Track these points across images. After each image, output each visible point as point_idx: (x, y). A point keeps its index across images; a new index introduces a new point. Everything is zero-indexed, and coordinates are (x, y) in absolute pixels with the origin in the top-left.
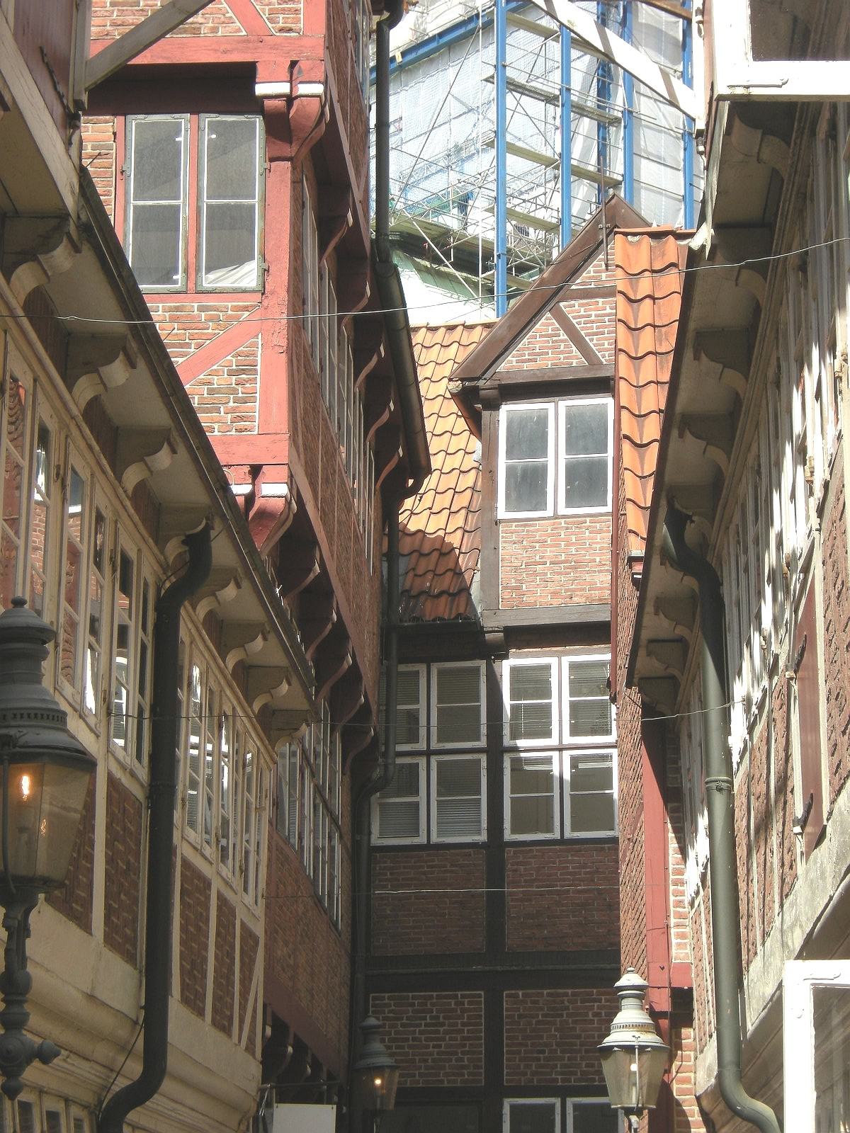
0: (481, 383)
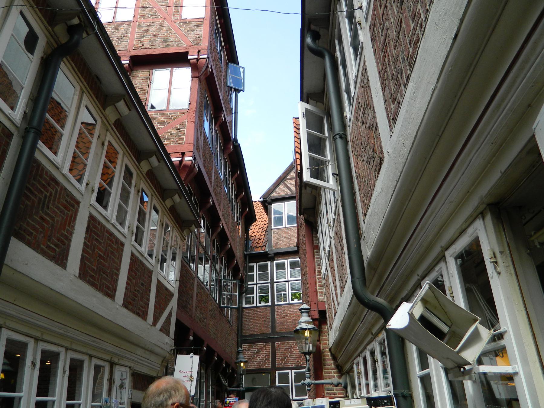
0: (267, 199)
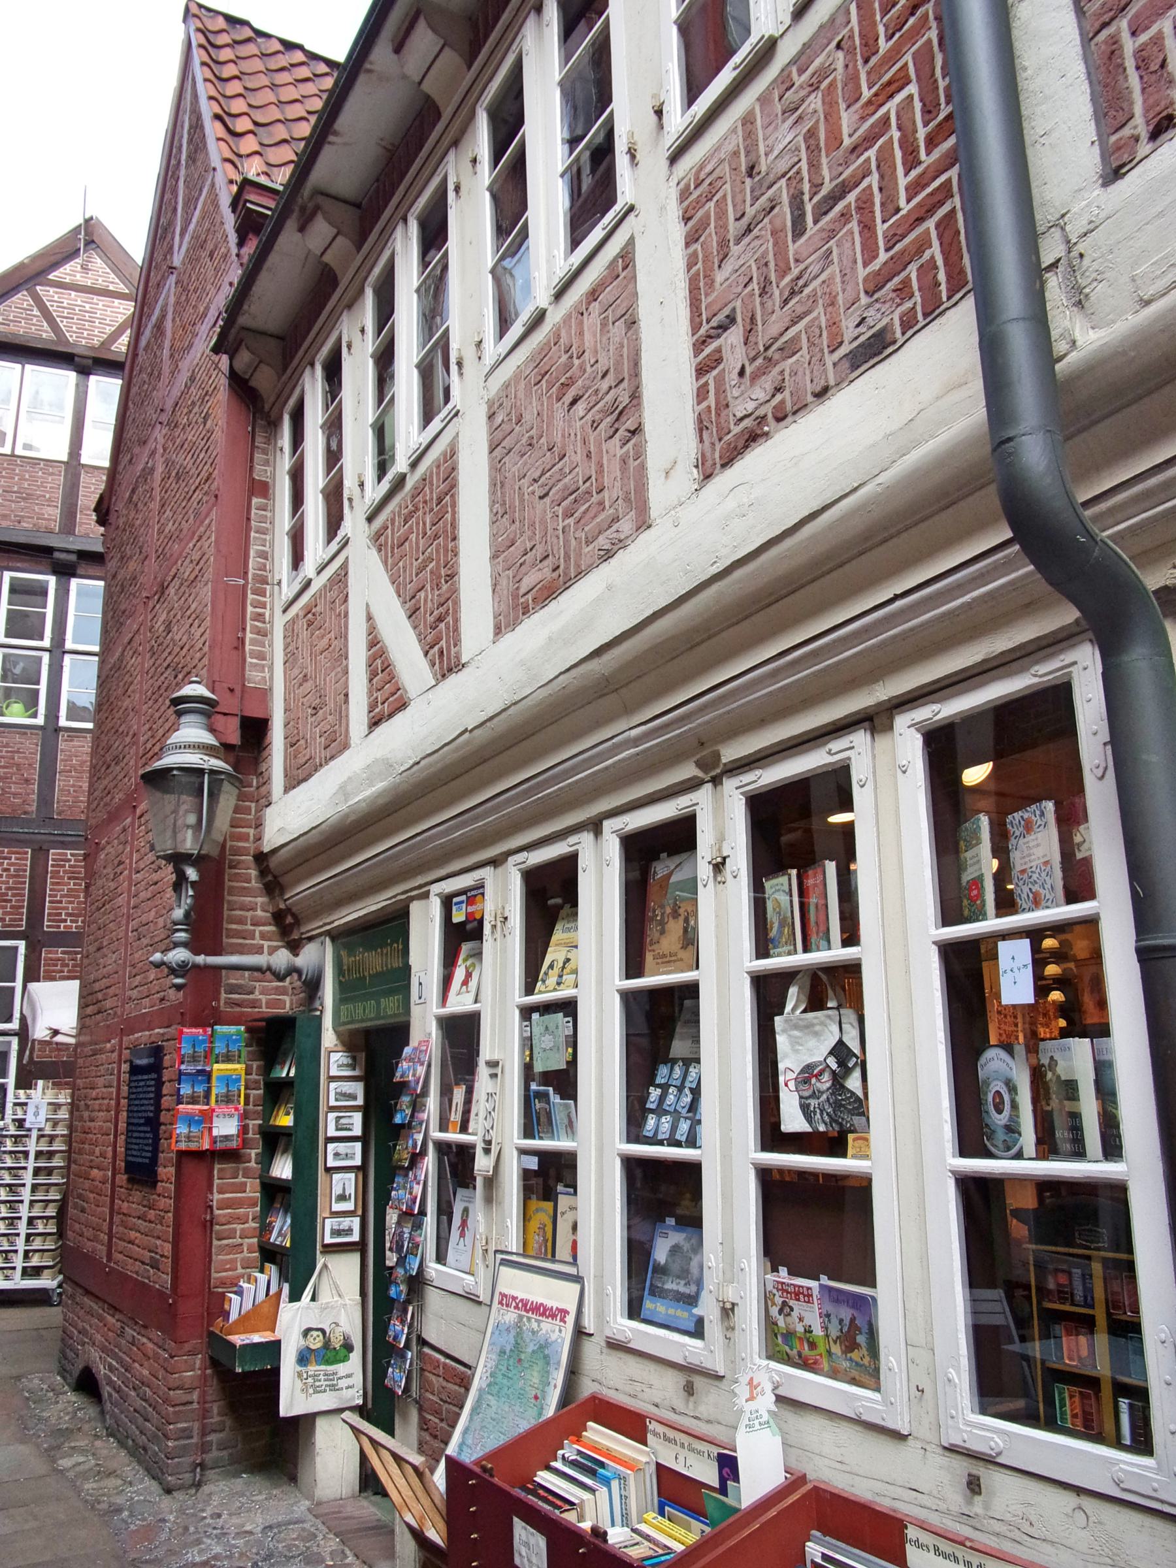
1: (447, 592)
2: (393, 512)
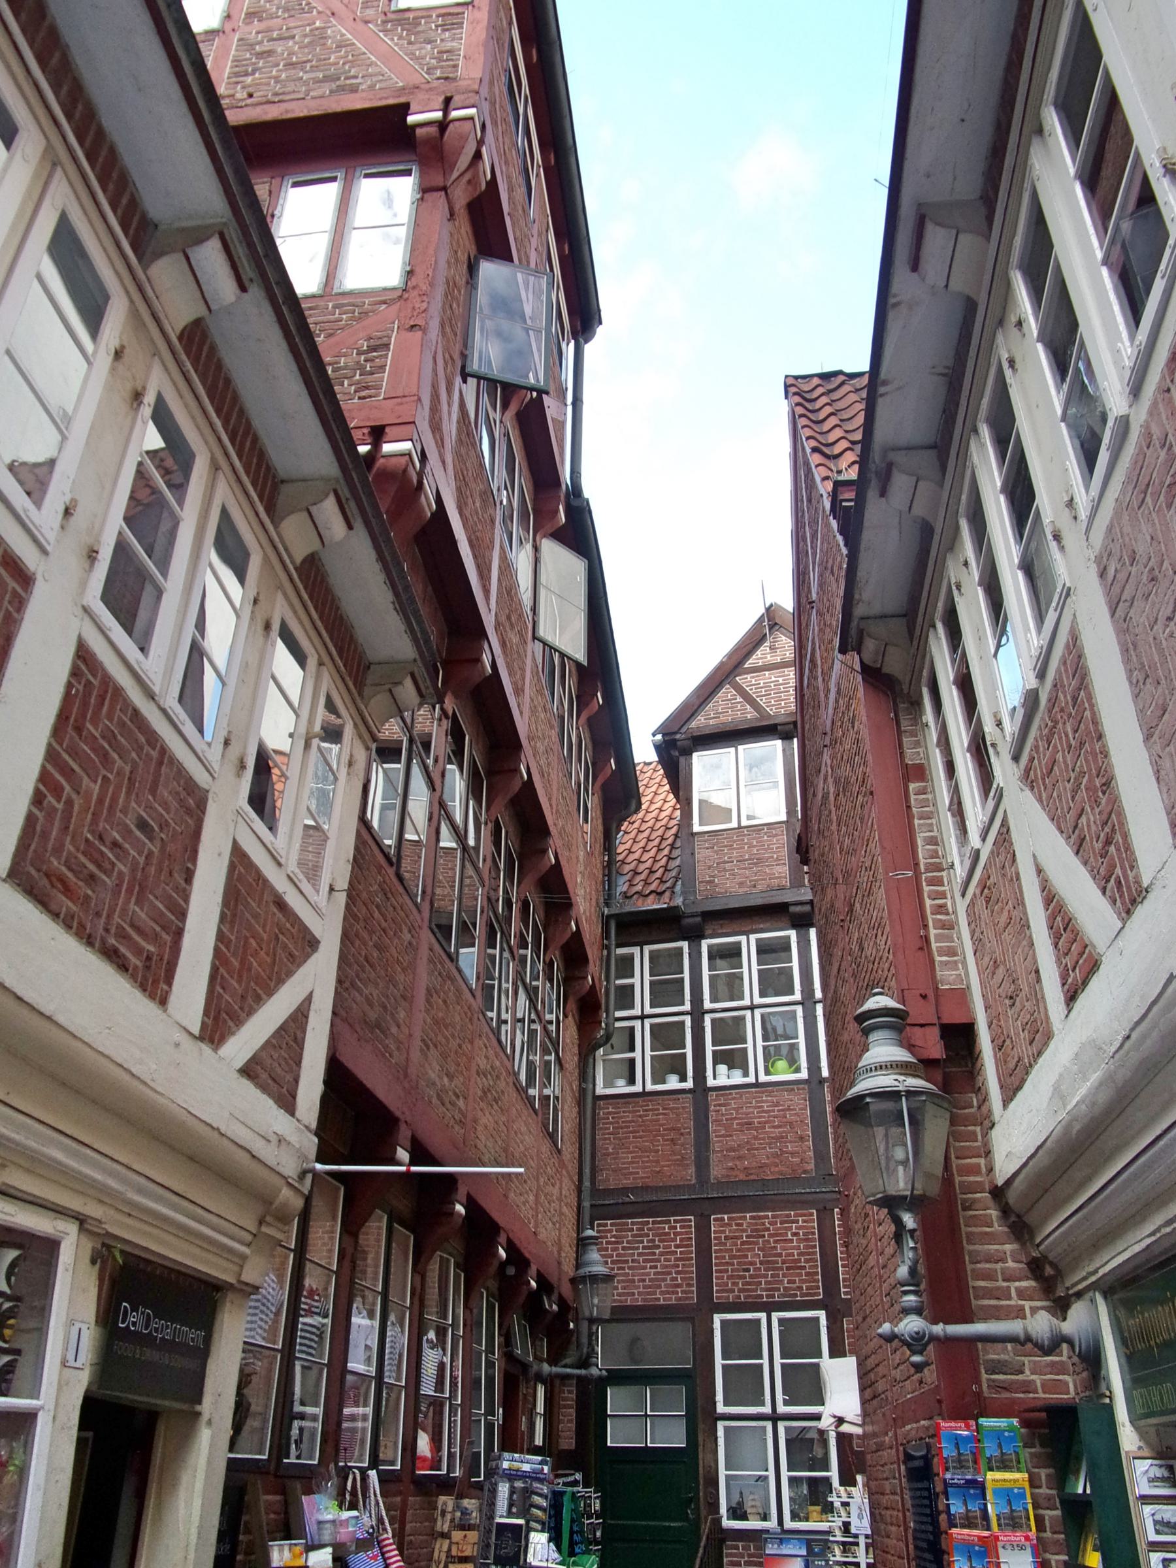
0: (678, 736)
1: (1107, 804)
2: (1036, 739)
